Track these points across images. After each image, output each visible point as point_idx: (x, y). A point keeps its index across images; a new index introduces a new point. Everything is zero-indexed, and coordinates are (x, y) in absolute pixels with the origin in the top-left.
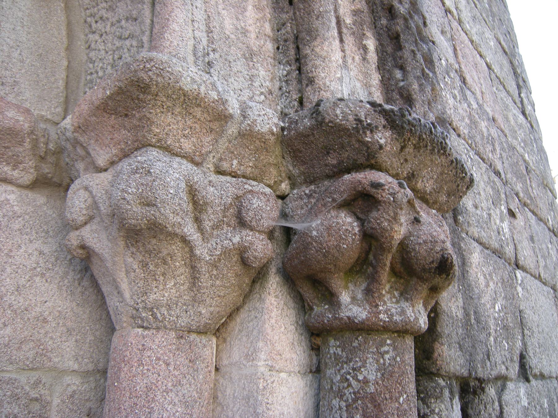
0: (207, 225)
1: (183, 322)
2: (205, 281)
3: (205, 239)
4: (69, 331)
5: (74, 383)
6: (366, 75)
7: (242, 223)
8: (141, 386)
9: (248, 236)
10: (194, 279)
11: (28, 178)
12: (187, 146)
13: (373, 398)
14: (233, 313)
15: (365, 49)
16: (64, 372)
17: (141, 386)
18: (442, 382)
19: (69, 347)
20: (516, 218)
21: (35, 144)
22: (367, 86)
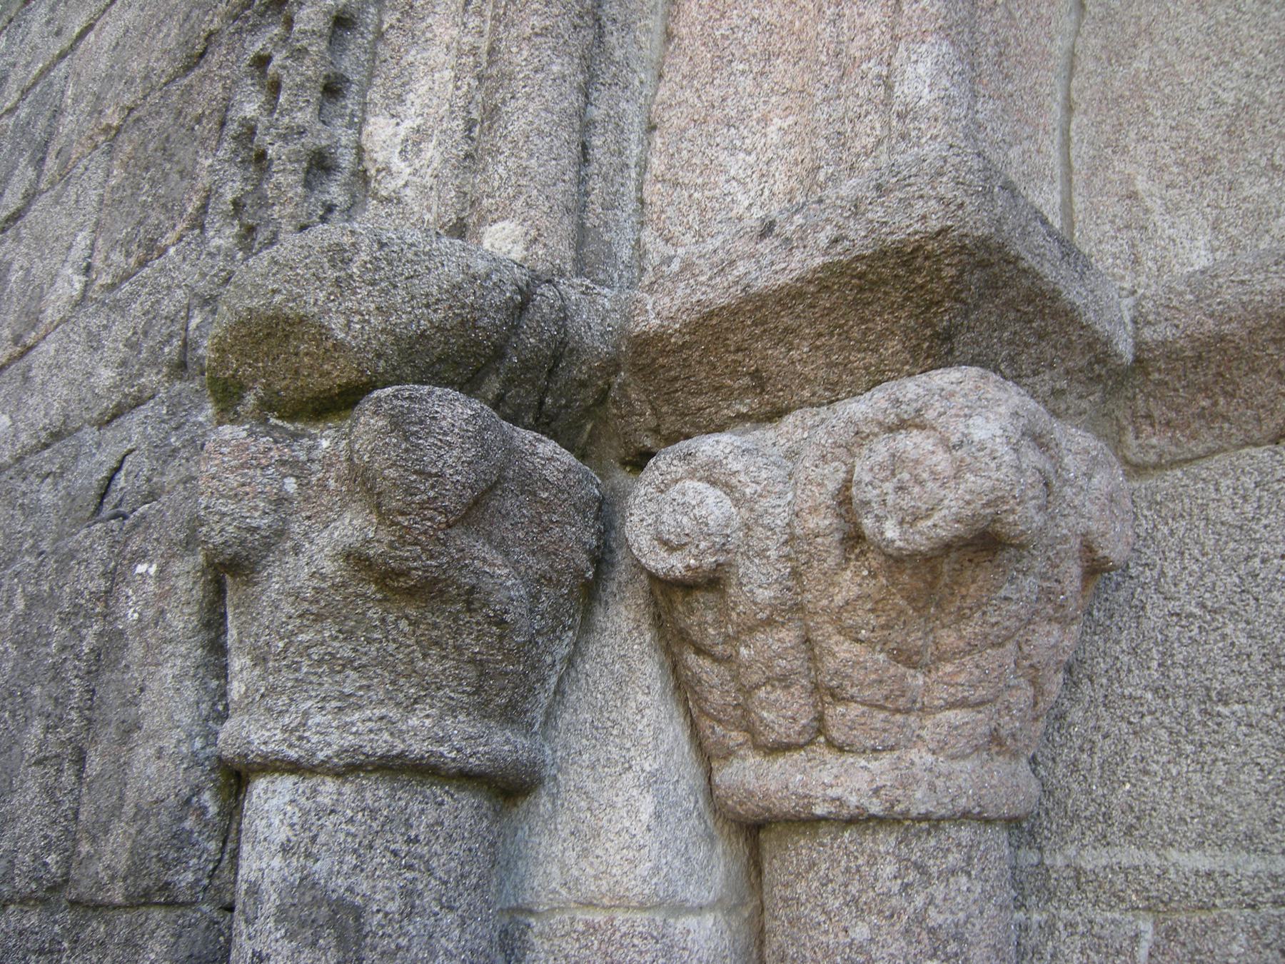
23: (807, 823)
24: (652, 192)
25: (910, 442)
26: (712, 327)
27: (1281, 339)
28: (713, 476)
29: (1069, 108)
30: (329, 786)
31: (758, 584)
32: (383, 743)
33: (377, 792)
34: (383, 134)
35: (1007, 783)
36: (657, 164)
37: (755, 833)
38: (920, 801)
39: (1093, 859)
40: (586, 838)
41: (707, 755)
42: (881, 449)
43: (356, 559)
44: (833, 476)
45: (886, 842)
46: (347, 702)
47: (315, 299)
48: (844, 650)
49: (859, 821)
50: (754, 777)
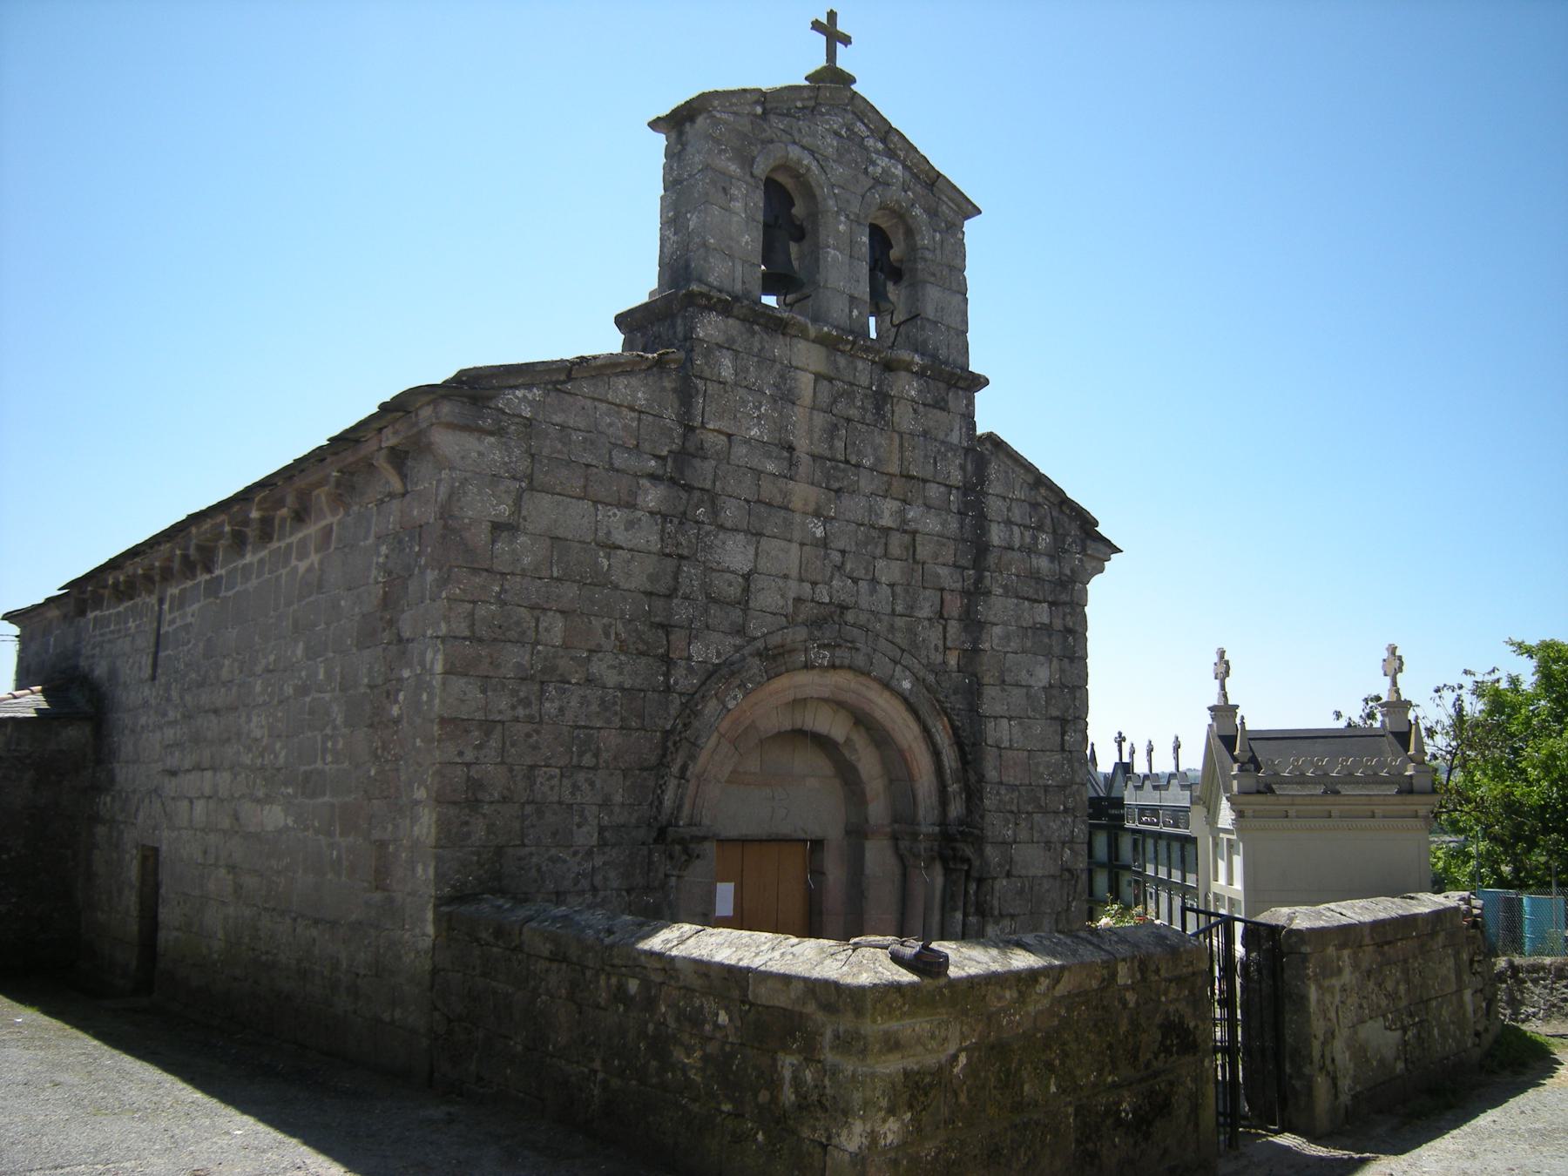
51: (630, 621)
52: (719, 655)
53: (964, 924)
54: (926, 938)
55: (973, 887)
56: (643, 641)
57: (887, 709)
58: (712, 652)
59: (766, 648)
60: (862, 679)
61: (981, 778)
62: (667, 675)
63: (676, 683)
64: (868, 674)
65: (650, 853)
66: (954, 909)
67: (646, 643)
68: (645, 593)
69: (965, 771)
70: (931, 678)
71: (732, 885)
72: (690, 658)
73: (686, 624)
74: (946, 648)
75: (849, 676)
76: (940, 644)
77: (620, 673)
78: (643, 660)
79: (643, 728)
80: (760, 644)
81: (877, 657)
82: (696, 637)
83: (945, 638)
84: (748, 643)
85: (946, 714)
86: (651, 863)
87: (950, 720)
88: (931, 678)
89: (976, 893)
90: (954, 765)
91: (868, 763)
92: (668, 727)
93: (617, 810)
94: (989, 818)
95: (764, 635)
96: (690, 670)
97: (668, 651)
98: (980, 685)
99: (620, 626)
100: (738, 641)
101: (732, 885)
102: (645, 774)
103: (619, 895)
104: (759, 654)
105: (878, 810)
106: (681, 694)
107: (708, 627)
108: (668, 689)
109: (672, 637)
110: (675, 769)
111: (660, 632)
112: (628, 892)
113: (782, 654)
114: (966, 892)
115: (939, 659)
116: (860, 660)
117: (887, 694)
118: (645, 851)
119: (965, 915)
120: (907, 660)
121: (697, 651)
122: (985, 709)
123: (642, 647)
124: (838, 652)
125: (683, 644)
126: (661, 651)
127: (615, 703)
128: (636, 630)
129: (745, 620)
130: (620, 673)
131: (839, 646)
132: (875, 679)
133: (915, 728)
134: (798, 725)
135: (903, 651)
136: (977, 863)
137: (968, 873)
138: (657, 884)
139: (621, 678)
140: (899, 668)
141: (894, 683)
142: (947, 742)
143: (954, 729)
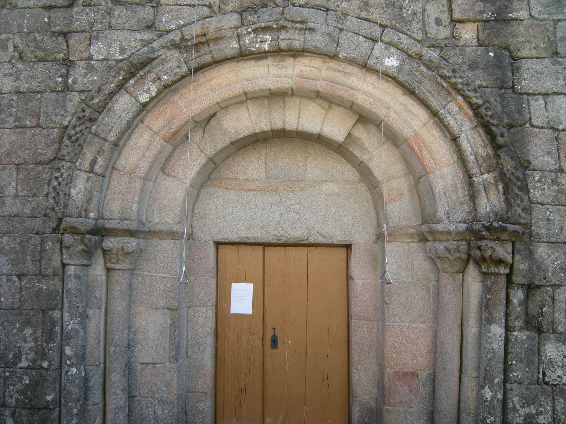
0: (451, 253)
1: (451, 271)
2: (453, 263)
3: (452, 256)
4: (432, 272)
5: (434, 283)
6: (499, 198)
7: (459, 252)
8: (444, 284)
9: (461, 254)
10: (451, 263)
11: (417, 241)
12: (444, 239)
13: (489, 288)
14: (465, 268)
15: (498, 189)
16: (432, 281)
17: (444, 284)
18: (514, 285)
19: (432, 275)
20: (277, 348)
21: (417, 234)
22: (499, 201)
23: (115, 269)
24: (105, 205)
25: (129, 245)
26: (112, 229)
27: (2, 406)
28: (111, 242)
29: (150, 197)
30: (77, 267)
31: (114, 252)
32: (83, 263)
33: (81, 267)
34: (73, 192)
35: (132, 267)
36: (106, 202)
37: (108, 270)
38: (124, 268)
39: (138, 272)
40: (94, 270)
41: (105, 263)
42: (126, 244)
43: (83, 250)
44: (122, 245)
45: (121, 271)
46: (79, 260)
47: (80, 227)
48: (120, 257)
49: (119, 270)
50: (110, 265)
51: (29, 33)
52: (122, 50)
53: (507, 341)
54: (185, 263)
55: (518, 296)
56: (41, 49)
57: (370, 92)
58: (115, 49)
59: (183, 39)
60: (333, 64)
61: (525, 165)
62: (66, 76)
63: (75, 82)
64: (334, 57)
65: (43, 241)
66: (490, 321)
67: (45, 50)
68: (44, 8)
69: (497, 156)
70: (433, 54)
71: (231, 312)
72: (90, 58)
73: (86, 28)
74: (454, 22)
75: (317, 62)
76: (445, 18)
77: (17, 79)
78: (41, 65)
79: (38, 126)
80: (176, 36)
81: (344, 38)
82: (97, 38)
83: (451, 10)
84: (160, 36)
85: (458, 91)
86: (43, 251)
87: (465, 98)
88: (433, 54)
89: (525, 303)
90: (482, 152)
91: (382, 160)
92: (66, 123)
93: (9, 201)
94: (538, 212)
95: (180, 27)
96: (90, 69)
97: (68, 53)
98: (515, 59)
99: (17, 38)
100: (147, 35)
101: (231, 312)
102: (40, 168)
103: (9, 280)
104: (175, 46)
105: (400, 210)
106: (80, 92)
107: (110, 27)
108: (67, 88)
109: (71, 42)
110: (86, 165)
111: (61, 39)
112: (20, 276)
113: (207, 43)
114: (508, 301)
115: (444, 32)
116: (317, 40)
117: (371, 78)
118: (37, 239)
119: (508, 329)
120: (390, 35)
121: (98, 50)
122: (527, 83)
123: (40, 54)
124: (283, 35)
125: (82, 47)
126: (61, 56)
127: (11, 106)
128: (35, 40)
129: (155, 16)
130: (17, 79)
131: (284, 27)
132: (352, 62)
133: (421, 114)
134: (279, 125)
135: (384, 27)
136: (522, 266)
137: (509, 277)
138: (50, 271)
139: (17, 84)
140: (379, 47)
141: (372, 62)
142: (467, 125)
143: (475, 108)
